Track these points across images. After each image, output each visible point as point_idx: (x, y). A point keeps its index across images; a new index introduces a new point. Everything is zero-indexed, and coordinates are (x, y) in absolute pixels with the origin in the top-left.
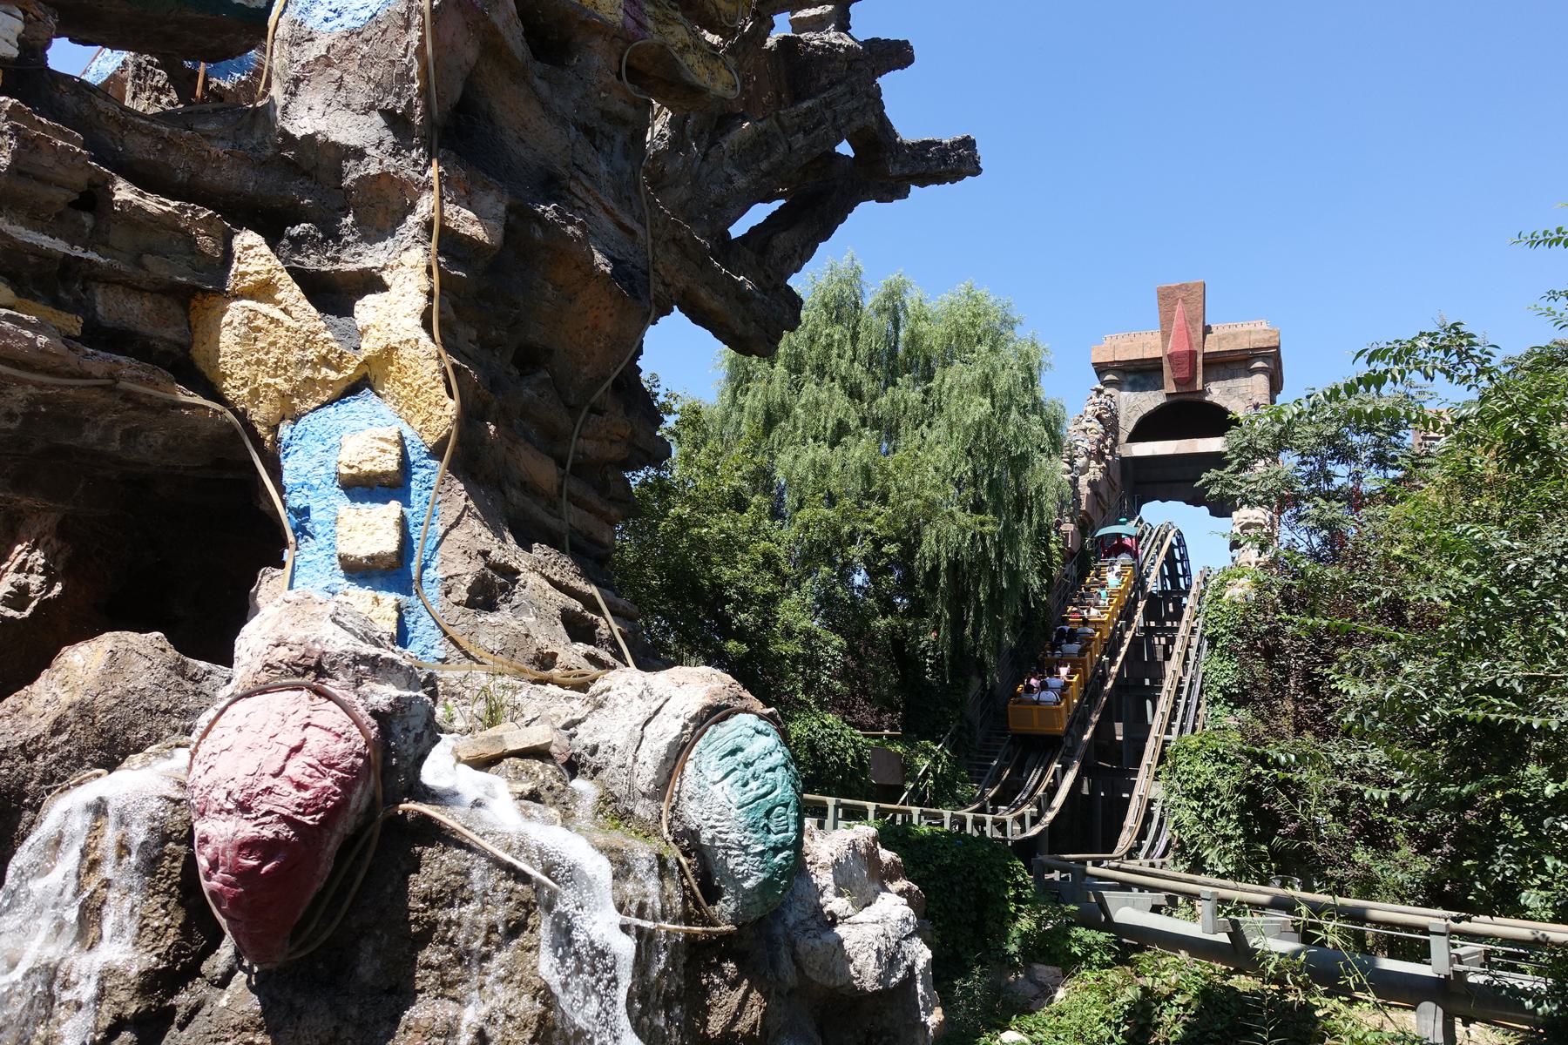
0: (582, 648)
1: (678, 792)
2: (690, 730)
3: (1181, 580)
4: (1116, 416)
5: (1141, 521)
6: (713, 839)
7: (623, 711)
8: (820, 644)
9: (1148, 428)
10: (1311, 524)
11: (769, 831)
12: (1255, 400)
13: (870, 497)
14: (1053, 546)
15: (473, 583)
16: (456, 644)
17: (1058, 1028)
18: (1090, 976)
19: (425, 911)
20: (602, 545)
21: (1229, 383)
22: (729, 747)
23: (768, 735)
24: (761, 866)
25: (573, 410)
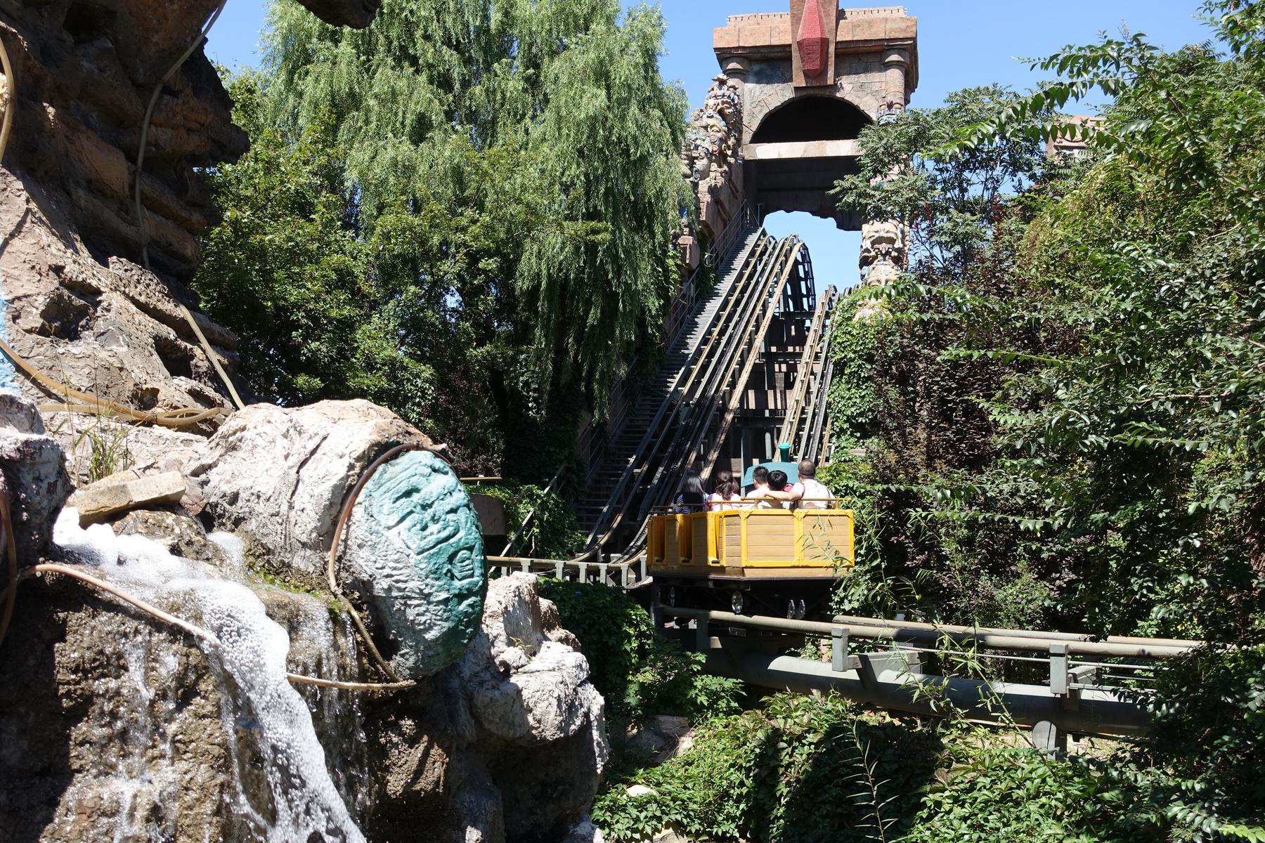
0: (184, 383)
1: (345, 541)
2: (357, 470)
3: (805, 300)
4: (740, 112)
5: (764, 233)
6: (390, 589)
7: (264, 453)
8: (407, 375)
9: (772, 128)
10: (945, 238)
11: (453, 577)
12: (889, 99)
13: (463, 202)
14: (670, 262)
15: (48, 306)
16: (34, 381)
17: (687, 778)
18: (719, 723)
19: (78, 683)
20: (183, 259)
21: (862, 78)
22: (404, 487)
23: (446, 473)
24: (445, 615)
25: (142, 89)
